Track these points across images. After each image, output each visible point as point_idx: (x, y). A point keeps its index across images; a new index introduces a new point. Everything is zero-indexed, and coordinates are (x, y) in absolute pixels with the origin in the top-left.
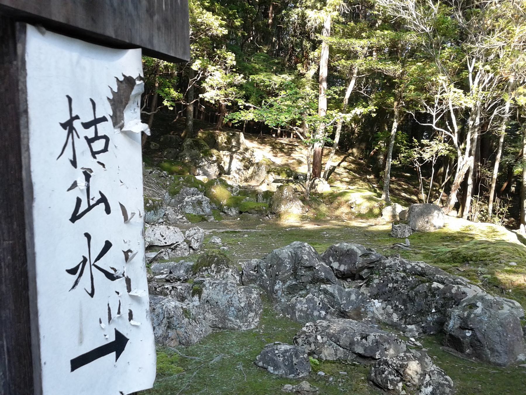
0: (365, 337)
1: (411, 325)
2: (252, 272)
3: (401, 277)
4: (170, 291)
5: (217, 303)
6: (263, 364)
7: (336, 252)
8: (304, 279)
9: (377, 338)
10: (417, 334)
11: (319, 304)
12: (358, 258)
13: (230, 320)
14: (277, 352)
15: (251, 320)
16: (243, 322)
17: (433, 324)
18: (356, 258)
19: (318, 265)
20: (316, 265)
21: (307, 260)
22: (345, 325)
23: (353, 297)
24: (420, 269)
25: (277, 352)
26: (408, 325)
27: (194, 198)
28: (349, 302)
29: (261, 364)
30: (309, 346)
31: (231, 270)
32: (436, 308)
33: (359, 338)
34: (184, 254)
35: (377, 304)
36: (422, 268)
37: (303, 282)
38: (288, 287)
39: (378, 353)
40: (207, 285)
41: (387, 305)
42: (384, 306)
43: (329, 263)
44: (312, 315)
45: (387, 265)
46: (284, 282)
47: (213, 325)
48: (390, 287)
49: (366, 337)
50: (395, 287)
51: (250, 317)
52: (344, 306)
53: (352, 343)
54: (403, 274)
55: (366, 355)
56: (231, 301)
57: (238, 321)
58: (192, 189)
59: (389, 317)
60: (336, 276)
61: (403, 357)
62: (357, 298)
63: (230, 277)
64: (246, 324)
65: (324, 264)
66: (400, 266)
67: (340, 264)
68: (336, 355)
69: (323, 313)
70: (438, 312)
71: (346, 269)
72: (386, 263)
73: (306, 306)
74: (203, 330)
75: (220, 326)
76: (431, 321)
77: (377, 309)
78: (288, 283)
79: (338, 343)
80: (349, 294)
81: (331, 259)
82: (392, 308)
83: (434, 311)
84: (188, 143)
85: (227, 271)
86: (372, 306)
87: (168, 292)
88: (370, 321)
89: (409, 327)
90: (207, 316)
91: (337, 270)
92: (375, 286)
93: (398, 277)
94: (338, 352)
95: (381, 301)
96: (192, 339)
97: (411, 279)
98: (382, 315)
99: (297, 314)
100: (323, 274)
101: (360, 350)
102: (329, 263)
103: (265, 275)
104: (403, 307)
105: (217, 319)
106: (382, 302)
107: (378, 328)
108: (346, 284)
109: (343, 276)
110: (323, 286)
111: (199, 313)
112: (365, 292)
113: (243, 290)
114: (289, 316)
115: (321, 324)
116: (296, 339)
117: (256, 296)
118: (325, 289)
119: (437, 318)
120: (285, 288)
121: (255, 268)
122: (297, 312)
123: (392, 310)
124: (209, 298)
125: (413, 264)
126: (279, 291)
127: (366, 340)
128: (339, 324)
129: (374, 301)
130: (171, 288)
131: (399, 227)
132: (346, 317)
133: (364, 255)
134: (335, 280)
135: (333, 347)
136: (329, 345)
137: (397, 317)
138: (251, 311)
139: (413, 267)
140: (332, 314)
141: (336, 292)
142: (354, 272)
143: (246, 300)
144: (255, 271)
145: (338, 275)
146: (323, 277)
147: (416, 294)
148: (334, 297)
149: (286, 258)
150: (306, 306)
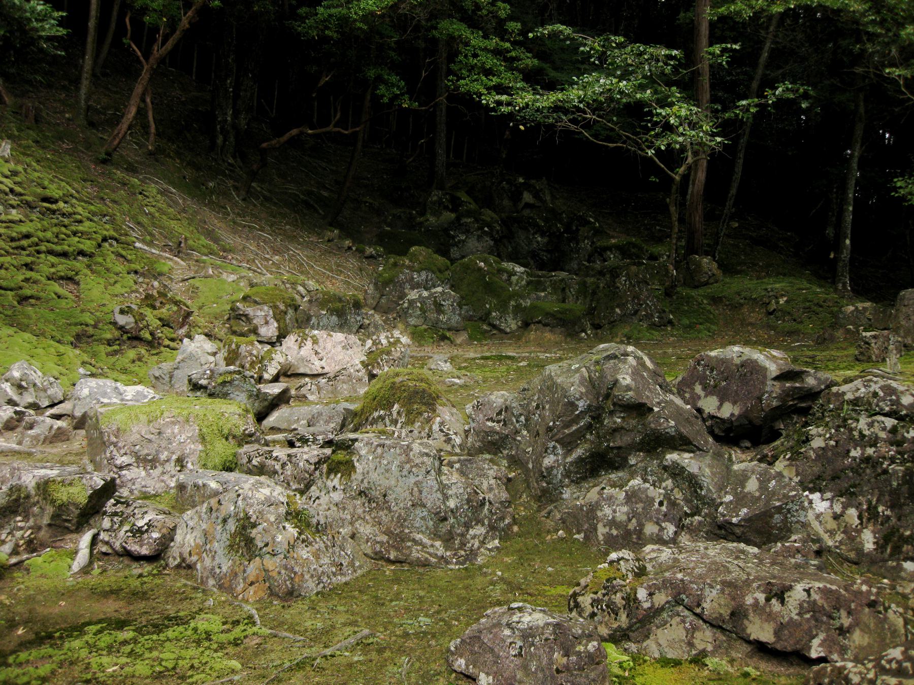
0: (780, 594)
2: (489, 424)
4: (283, 465)
5: (385, 496)
6: (467, 665)
7: (712, 370)
11: (661, 504)
12: (769, 383)
15: (477, 544)
18: (764, 383)
21: (628, 388)
22: (723, 558)
23: (752, 485)
26: (905, 560)
28: (741, 499)
29: (460, 663)
33: (761, 597)
34: (356, 391)
35: (820, 504)
39: (816, 642)
42: (838, 508)
44: (640, 532)
45: (849, 396)
47: (376, 553)
48: (854, 459)
49: (783, 593)
51: (474, 537)
53: (738, 614)
54: (890, 422)
55: (779, 647)
60: (711, 432)
61: (898, 662)
65: (678, 401)
68: (691, 644)
69: (671, 529)
71: (736, 413)
72: (844, 393)
79: (698, 611)
80: (743, 478)
81: (698, 389)
84: (435, 198)
91: (712, 417)
92: (812, 455)
93: (876, 429)
98: (832, 533)
99: (602, 530)
100: (672, 423)
102: (694, 399)
106: (831, 500)
107: (819, 568)
108: (736, 454)
109: (730, 435)
110: (672, 457)
111: (343, 520)
112: (785, 473)
113: (457, 466)
114: (580, 537)
115: (654, 555)
116: (575, 595)
117: (493, 482)
118: (675, 464)
120: (571, 463)
121: (499, 413)
122: (600, 526)
126: (555, 472)
127: (783, 602)
128: (706, 556)
129: (811, 497)
130: (286, 458)
131: (875, 337)
132: (731, 537)
133: (784, 376)
134: (706, 442)
135: (684, 622)
138: (479, 522)
140: (693, 531)
142: (758, 422)
143: (461, 491)
144: (498, 422)
145: (717, 431)
146: (672, 432)
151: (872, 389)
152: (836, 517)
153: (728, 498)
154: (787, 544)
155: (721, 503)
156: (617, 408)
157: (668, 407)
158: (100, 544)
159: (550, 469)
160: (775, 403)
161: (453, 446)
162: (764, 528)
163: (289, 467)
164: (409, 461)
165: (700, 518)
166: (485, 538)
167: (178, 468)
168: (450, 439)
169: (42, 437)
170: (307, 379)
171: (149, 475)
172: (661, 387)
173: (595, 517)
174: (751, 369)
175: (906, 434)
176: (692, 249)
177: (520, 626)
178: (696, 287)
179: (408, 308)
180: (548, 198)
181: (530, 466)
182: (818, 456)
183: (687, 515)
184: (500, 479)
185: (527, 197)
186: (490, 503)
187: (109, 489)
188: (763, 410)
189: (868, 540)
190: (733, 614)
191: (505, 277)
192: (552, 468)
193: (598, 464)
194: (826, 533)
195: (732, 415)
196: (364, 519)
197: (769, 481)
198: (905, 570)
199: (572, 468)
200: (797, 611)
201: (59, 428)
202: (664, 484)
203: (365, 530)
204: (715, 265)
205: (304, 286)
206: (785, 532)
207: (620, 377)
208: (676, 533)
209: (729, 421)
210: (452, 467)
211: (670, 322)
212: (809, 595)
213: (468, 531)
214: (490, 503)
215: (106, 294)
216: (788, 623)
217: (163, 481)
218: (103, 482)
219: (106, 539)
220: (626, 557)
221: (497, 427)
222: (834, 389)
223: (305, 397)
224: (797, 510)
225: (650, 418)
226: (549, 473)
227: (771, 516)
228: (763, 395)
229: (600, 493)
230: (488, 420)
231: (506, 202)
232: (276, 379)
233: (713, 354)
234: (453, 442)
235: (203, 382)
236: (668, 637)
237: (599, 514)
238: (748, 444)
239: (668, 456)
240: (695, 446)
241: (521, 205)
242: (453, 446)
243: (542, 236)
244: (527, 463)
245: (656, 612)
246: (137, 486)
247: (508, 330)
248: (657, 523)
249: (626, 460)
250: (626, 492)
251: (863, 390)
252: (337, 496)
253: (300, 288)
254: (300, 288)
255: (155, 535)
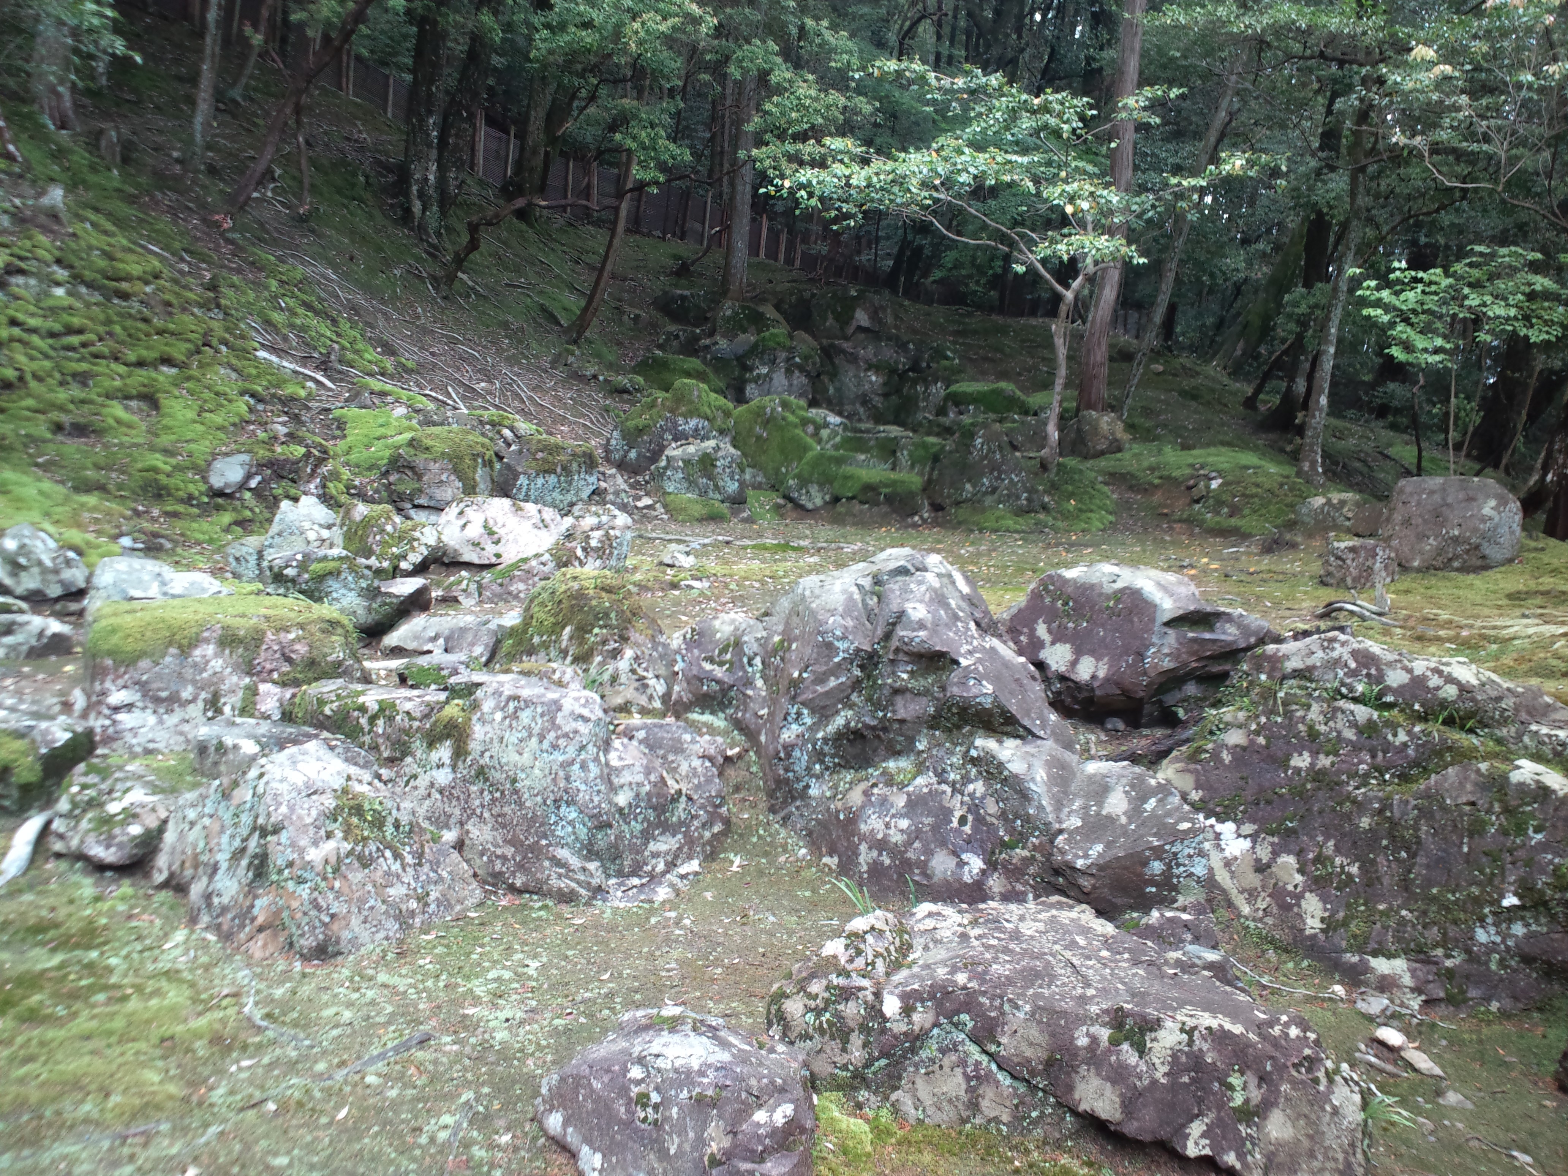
1: (1389, 956)
2: (708, 666)
3: (1354, 724)
8: (905, 709)
9: (1198, 1042)
10: (1415, 1003)
11: (963, 820)
13: (558, 862)
14: (636, 1072)
15: (661, 867)
16: (620, 874)
17: (1502, 963)
19: (970, 648)
20: (965, 648)
21: (921, 625)
24: (1450, 692)
25: (636, 1072)
26: (1375, 954)
27: (691, 449)
28: (1097, 826)
30: (836, 1045)
31: (629, 653)
32: (1525, 889)
35: (1233, 841)
36: (1464, 689)
37: (902, 721)
38: (839, 736)
39: (1196, 1128)
40: (487, 706)
41: (1275, 854)
42: (1264, 853)
43: (1031, 650)
46: (823, 713)
48: (1298, 770)
50: (1323, 772)
51: (656, 855)
52: (1068, 841)
54: (1362, 713)
55: (1131, 1129)
56: (567, 778)
57: (592, 866)
58: (693, 423)
59: (1285, 908)
62: (1135, 811)
63: (623, 679)
64: (636, 881)
66: (1353, 673)
67: (1079, 653)
69: (975, 863)
70: (1535, 906)
71: (1101, 674)
72: (1287, 657)
73: (904, 823)
74: (433, 895)
75: (518, 883)
76: (1492, 948)
77: (1228, 863)
78: (839, 721)
79: (993, 1048)
80: (1100, 789)
81: (1041, 630)
82: (1301, 871)
83: (1510, 900)
84: (729, 313)
85: (615, 654)
86: (1202, 854)
87: (363, 721)
88: (1186, 926)
89: (1381, 965)
90: (474, 832)
91: (1063, 678)
94: (988, 1093)
95: (1249, 828)
96: (346, 935)
97: (1402, 737)
98: (1251, 895)
100: (988, 688)
101: (1097, 1097)
103: (760, 683)
104: (1354, 869)
105: (509, 851)
106: (1254, 837)
110: (984, 743)
113: (641, 734)
115: (930, 924)
117: (696, 763)
119: (1529, 936)
120: (825, 740)
122: (863, 848)
123: (1299, 878)
124: (486, 760)
125: (1420, 666)
126: (797, 753)
127: (1141, 1050)
129: (1219, 827)
136: (944, 1051)
137: (1319, 913)
138: (668, 828)
139: (1418, 682)
141: (1041, 774)
143: (640, 778)
146: (988, 703)
147: (1424, 813)
148: (1024, 796)
149: (832, 612)
150: (904, 823)
151: (1335, 654)
152: (1261, 868)
153: (1075, 822)
154: (1169, 914)
155: (1061, 831)
156: (901, 656)
157: (985, 664)
158: (52, 839)
159: (789, 748)
160: (1167, 664)
161: (651, 698)
162: (1123, 890)
163: (380, 722)
164: (555, 726)
165: (1026, 853)
166: (676, 857)
167: (210, 714)
168: (646, 686)
169: (25, 648)
170: (464, 573)
171: (161, 722)
172: (978, 624)
173: (855, 832)
174: (1134, 604)
175: (1390, 737)
176: (1086, 401)
177: (660, 1063)
178: (1086, 457)
179: (665, 468)
180: (890, 320)
181: (763, 738)
182: (1235, 759)
183: (1004, 846)
184: (711, 759)
185: (862, 317)
186: (690, 799)
187: (82, 747)
188: (1145, 673)
189: (1313, 913)
190: (1050, 1063)
191: (810, 429)
192: (793, 746)
193: (857, 749)
194: (1241, 892)
195: (1094, 677)
196: (481, 817)
197: (1145, 800)
198: (1372, 970)
199: (826, 749)
200: (1165, 1069)
201: (55, 635)
202: (971, 787)
203: (481, 833)
204: (1120, 426)
205: (512, 429)
206: (1167, 890)
207: (909, 606)
208: (983, 872)
209: (1087, 687)
210: (631, 738)
211: (1045, 508)
212: (1191, 1042)
213: (646, 844)
214: (690, 799)
215: (200, 430)
216: (1146, 1089)
217: (181, 733)
218: (68, 735)
219: (62, 830)
220: (879, 925)
221: (719, 672)
222: (1271, 648)
223: (456, 600)
224: (1190, 856)
225: (955, 676)
226: (789, 756)
227: (1145, 863)
228: (1147, 648)
229: (867, 794)
230: (706, 659)
231: (830, 322)
232: (420, 569)
233: (1070, 574)
234: (649, 691)
235: (290, 572)
236: (932, 1092)
237: (863, 827)
238: (1121, 726)
239: (979, 742)
240: (1025, 728)
241: (850, 330)
242: (651, 698)
243: (877, 373)
244: (759, 733)
245: (917, 1039)
246: (140, 739)
247: (810, 506)
248: (955, 854)
249: (911, 741)
250: (908, 794)
251: (1320, 654)
252: (443, 777)
253: (507, 432)
254: (507, 432)
255: (135, 830)
